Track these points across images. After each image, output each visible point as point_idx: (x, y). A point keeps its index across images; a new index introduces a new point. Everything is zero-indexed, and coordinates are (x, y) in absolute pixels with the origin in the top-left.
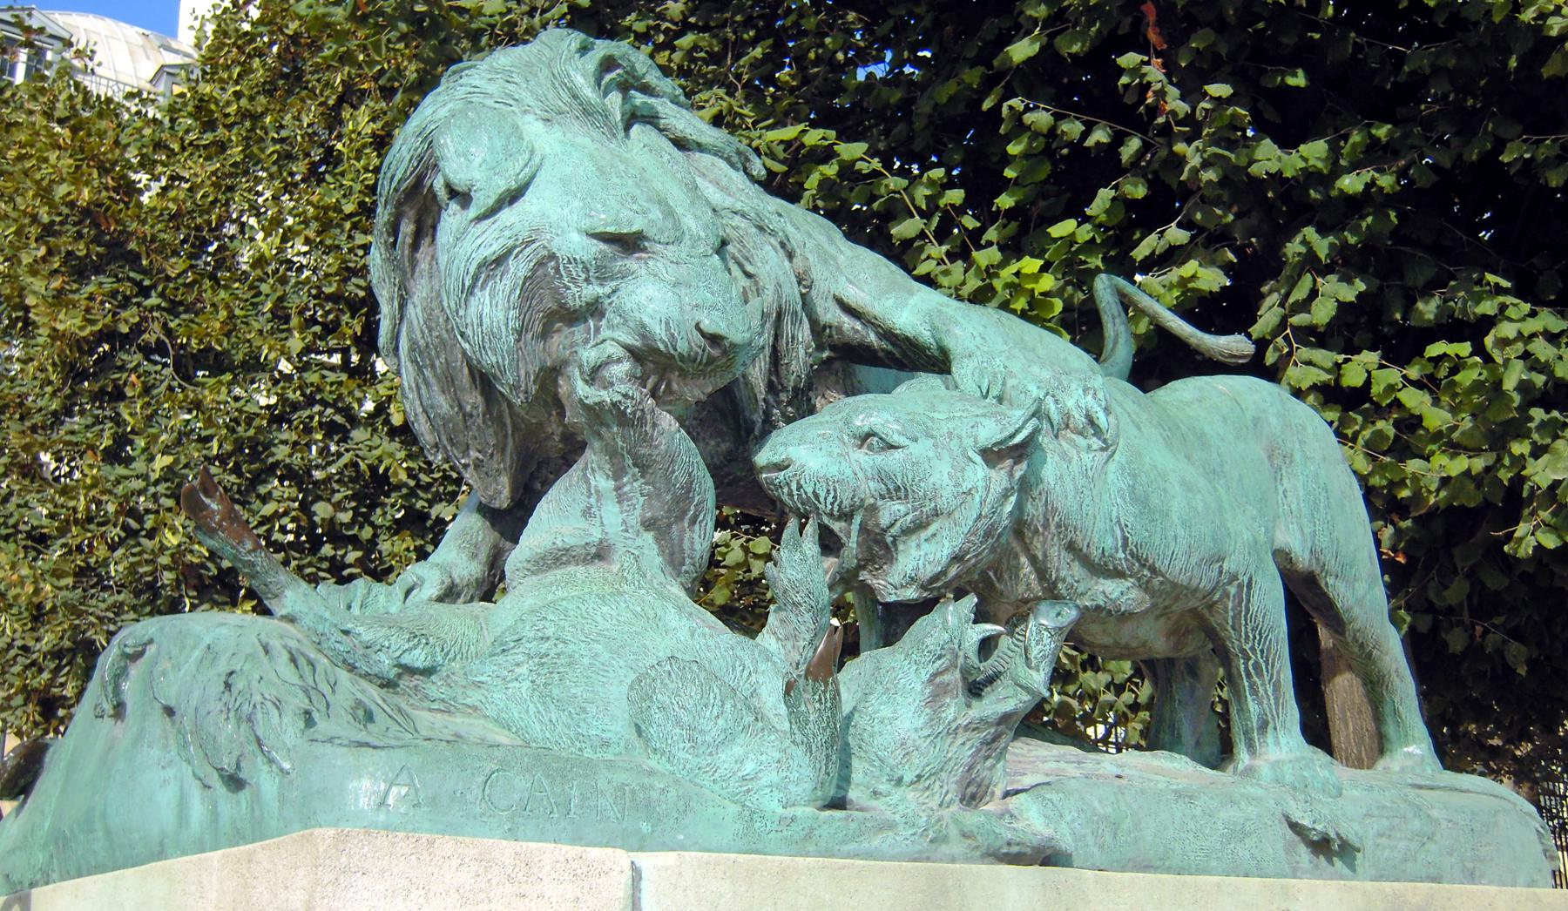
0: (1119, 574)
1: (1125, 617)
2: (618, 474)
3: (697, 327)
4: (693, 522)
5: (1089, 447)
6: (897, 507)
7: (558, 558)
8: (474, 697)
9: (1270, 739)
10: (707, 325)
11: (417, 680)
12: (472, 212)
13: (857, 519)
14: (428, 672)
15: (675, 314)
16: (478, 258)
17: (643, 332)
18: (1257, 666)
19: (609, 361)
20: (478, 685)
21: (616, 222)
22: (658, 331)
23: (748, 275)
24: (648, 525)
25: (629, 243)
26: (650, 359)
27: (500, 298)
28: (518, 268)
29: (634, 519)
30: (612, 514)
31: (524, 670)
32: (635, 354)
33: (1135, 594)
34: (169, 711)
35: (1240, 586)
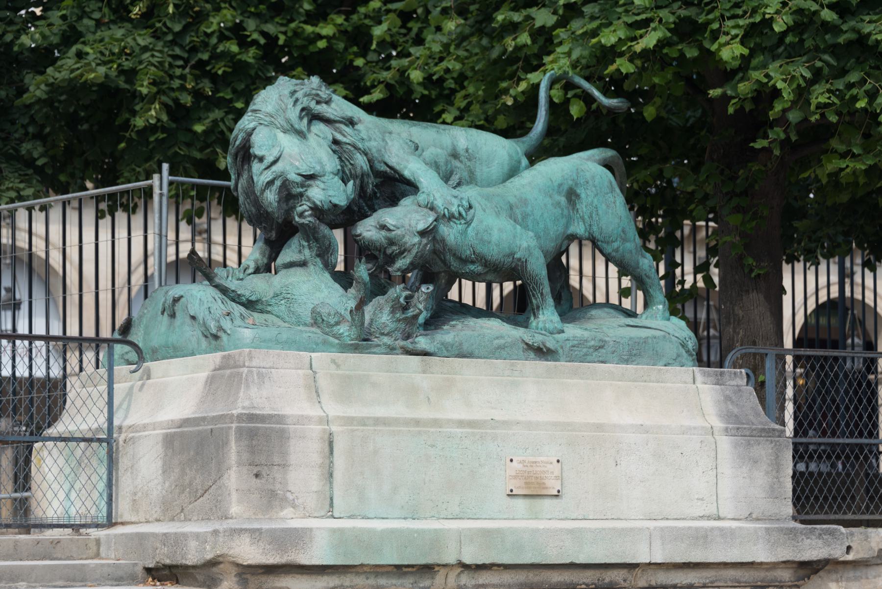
0: (473, 262)
2: (308, 241)
6: (394, 248)
7: (290, 265)
8: (269, 309)
9: (541, 312)
12: (263, 166)
15: (323, 198)
17: (314, 203)
19: (305, 211)
22: (318, 203)
23: (351, 164)
24: (318, 255)
25: (312, 177)
26: (317, 211)
28: (278, 183)
29: (314, 254)
30: (307, 252)
31: (282, 302)
32: (311, 208)
33: (480, 268)
34: (193, 318)
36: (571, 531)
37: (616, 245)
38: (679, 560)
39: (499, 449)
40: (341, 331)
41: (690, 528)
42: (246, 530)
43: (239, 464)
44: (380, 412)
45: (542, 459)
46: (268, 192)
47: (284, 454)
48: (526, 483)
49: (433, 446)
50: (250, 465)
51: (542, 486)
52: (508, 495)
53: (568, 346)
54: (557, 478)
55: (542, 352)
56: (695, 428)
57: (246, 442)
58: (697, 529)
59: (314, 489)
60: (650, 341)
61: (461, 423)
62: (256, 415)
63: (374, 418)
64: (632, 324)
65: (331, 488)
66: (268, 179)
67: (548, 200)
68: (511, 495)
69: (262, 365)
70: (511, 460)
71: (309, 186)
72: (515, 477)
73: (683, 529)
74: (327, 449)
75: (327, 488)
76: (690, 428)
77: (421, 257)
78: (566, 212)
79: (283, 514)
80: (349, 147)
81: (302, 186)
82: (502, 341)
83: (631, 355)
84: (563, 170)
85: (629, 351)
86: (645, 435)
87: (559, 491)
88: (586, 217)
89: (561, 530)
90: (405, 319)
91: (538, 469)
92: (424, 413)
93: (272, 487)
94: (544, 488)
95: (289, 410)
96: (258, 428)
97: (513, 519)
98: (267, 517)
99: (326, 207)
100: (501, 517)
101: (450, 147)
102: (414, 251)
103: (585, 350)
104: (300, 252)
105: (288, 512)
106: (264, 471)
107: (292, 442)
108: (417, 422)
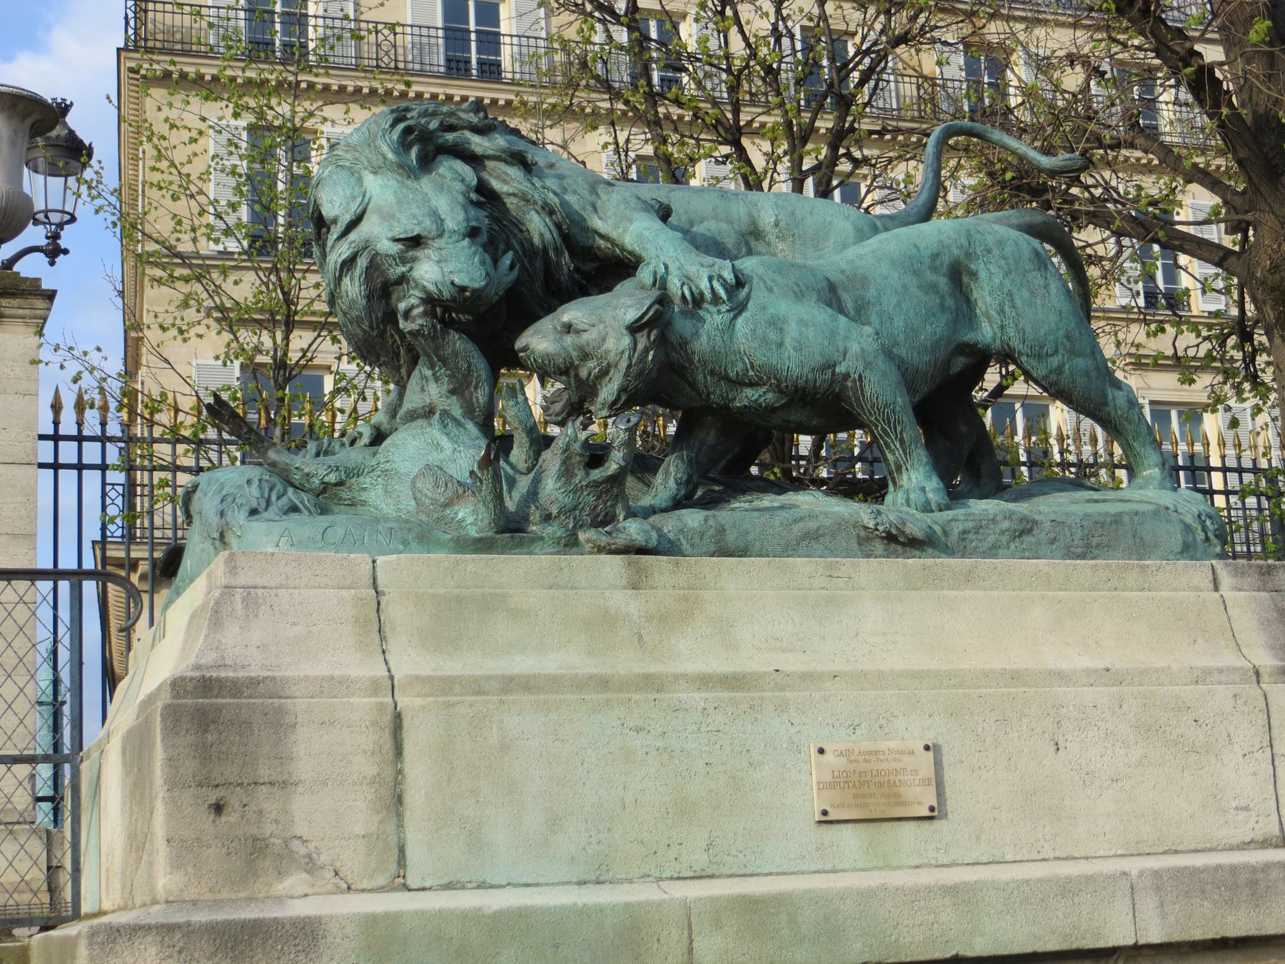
0: (752, 385)
1: (771, 410)
2: (432, 367)
3: (452, 283)
4: (476, 388)
5: (719, 311)
10: (457, 281)
11: (335, 490)
13: (572, 373)
14: (340, 484)
16: (340, 260)
17: (424, 289)
18: (883, 429)
19: (413, 307)
20: (365, 489)
21: (405, 232)
22: (432, 288)
24: (453, 392)
25: (415, 242)
27: (356, 279)
28: (362, 262)
35: (854, 381)
36: (952, 891)
37: (1055, 361)
38: (1198, 934)
39: (793, 730)
40: (460, 515)
41: (1218, 868)
42: (148, 928)
43: (173, 784)
44: (522, 664)
45: (892, 744)
46: (346, 281)
47: (283, 759)
48: (856, 796)
49: (639, 730)
50: (200, 785)
51: (898, 800)
52: (821, 822)
53: (956, 532)
54: (925, 782)
55: (899, 542)
56: (1220, 671)
57: (191, 738)
58: (1234, 870)
59: (359, 829)
60: (1126, 519)
61: (703, 681)
62: (218, 680)
63: (503, 677)
64: (1121, 504)
65: (400, 826)
66: (344, 257)
67: (909, 280)
68: (826, 820)
69: (259, 582)
70: (821, 751)
71: (414, 260)
72: (831, 785)
73: (1205, 869)
74: (388, 745)
75: (391, 827)
76: (1208, 672)
77: (640, 374)
78: (950, 302)
79: (281, 888)
80: (515, 200)
81: (404, 261)
82: (812, 525)
83: (1088, 546)
84: (940, 232)
85: (1086, 538)
86: (1114, 689)
87: (932, 809)
88: (993, 313)
89: (929, 889)
90: (596, 484)
91: (884, 766)
92: (627, 663)
93: (255, 831)
94: (897, 804)
95: (302, 668)
96: (220, 709)
97: (834, 871)
98: (242, 895)
99: (446, 294)
100: (805, 867)
101: (745, 219)
102: (623, 365)
103: (991, 539)
104: (423, 389)
105: (295, 882)
106: (235, 799)
107: (302, 734)
108: (603, 683)
